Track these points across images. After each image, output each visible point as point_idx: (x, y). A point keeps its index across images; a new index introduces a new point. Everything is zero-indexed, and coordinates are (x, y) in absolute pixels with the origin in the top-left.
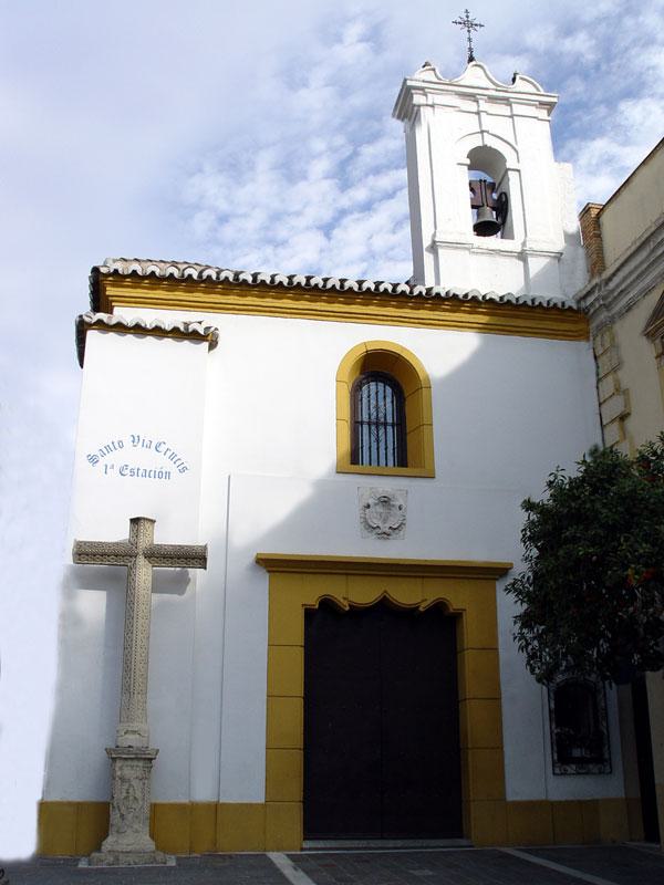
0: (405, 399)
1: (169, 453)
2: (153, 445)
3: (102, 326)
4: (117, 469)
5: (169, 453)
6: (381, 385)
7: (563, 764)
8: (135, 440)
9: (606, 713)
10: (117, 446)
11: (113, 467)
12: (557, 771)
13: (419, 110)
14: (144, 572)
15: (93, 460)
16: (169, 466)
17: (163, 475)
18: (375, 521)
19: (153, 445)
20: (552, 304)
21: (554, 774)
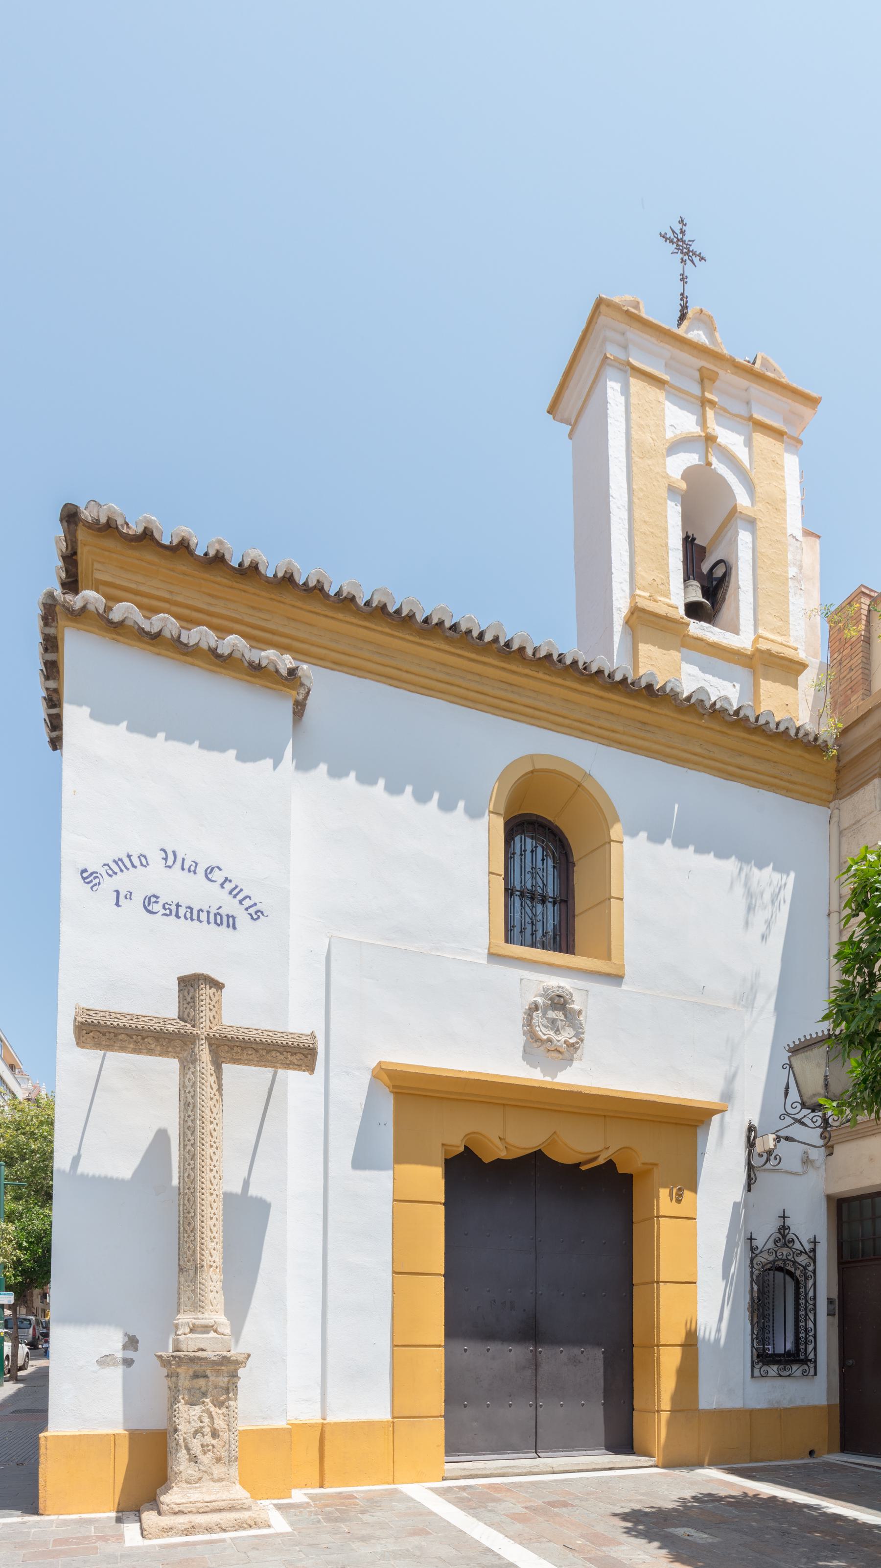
0: (574, 864)
1: (228, 886)
2: (201, 870)
3: (80, 615)
4: (138, 898)
5: (228, 886)
6: (529, 841)
7: (764, 1364)
8: (170, 858)
9: (815, 1305)
10: (136, 862)
11: (129, 896)
12: (757, 1373)
13: (659, 1351)
14: (536, 825)
15: (88, 877)
16: (230, 906)
17: (231, 922)
18: (543, 1029)
19: (201, 870)
20: (782, 728)
21: (753, 1376)
